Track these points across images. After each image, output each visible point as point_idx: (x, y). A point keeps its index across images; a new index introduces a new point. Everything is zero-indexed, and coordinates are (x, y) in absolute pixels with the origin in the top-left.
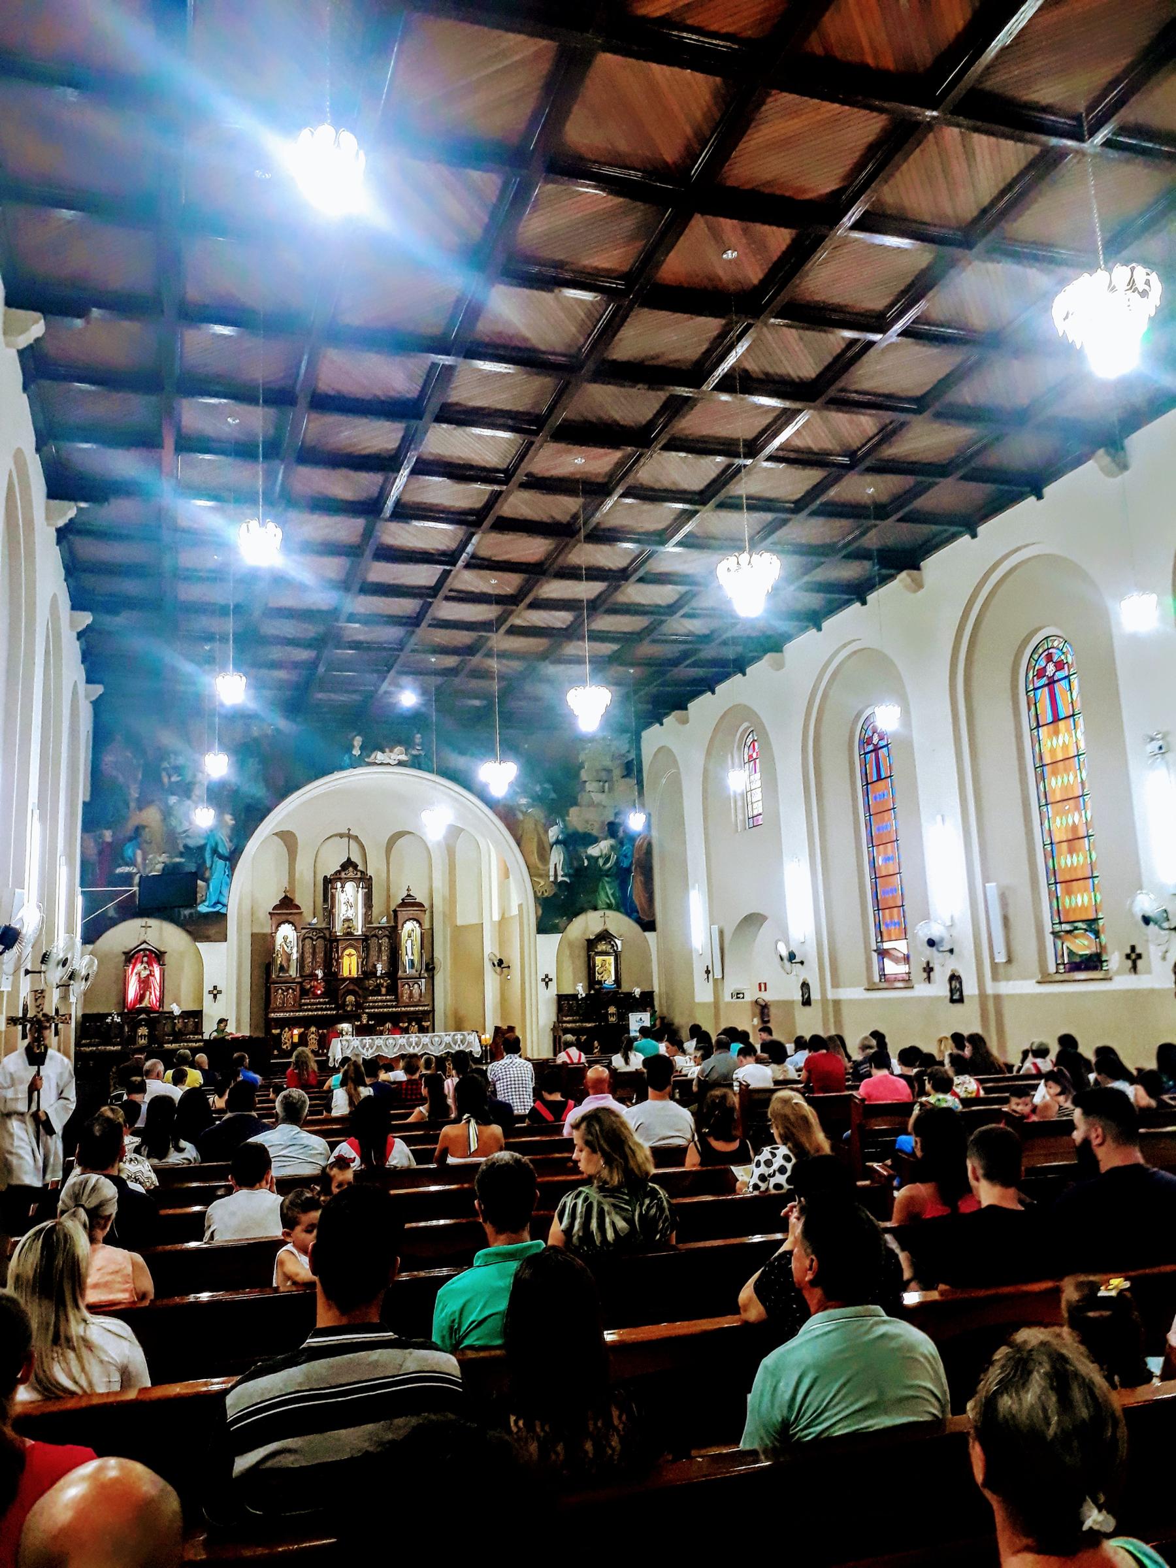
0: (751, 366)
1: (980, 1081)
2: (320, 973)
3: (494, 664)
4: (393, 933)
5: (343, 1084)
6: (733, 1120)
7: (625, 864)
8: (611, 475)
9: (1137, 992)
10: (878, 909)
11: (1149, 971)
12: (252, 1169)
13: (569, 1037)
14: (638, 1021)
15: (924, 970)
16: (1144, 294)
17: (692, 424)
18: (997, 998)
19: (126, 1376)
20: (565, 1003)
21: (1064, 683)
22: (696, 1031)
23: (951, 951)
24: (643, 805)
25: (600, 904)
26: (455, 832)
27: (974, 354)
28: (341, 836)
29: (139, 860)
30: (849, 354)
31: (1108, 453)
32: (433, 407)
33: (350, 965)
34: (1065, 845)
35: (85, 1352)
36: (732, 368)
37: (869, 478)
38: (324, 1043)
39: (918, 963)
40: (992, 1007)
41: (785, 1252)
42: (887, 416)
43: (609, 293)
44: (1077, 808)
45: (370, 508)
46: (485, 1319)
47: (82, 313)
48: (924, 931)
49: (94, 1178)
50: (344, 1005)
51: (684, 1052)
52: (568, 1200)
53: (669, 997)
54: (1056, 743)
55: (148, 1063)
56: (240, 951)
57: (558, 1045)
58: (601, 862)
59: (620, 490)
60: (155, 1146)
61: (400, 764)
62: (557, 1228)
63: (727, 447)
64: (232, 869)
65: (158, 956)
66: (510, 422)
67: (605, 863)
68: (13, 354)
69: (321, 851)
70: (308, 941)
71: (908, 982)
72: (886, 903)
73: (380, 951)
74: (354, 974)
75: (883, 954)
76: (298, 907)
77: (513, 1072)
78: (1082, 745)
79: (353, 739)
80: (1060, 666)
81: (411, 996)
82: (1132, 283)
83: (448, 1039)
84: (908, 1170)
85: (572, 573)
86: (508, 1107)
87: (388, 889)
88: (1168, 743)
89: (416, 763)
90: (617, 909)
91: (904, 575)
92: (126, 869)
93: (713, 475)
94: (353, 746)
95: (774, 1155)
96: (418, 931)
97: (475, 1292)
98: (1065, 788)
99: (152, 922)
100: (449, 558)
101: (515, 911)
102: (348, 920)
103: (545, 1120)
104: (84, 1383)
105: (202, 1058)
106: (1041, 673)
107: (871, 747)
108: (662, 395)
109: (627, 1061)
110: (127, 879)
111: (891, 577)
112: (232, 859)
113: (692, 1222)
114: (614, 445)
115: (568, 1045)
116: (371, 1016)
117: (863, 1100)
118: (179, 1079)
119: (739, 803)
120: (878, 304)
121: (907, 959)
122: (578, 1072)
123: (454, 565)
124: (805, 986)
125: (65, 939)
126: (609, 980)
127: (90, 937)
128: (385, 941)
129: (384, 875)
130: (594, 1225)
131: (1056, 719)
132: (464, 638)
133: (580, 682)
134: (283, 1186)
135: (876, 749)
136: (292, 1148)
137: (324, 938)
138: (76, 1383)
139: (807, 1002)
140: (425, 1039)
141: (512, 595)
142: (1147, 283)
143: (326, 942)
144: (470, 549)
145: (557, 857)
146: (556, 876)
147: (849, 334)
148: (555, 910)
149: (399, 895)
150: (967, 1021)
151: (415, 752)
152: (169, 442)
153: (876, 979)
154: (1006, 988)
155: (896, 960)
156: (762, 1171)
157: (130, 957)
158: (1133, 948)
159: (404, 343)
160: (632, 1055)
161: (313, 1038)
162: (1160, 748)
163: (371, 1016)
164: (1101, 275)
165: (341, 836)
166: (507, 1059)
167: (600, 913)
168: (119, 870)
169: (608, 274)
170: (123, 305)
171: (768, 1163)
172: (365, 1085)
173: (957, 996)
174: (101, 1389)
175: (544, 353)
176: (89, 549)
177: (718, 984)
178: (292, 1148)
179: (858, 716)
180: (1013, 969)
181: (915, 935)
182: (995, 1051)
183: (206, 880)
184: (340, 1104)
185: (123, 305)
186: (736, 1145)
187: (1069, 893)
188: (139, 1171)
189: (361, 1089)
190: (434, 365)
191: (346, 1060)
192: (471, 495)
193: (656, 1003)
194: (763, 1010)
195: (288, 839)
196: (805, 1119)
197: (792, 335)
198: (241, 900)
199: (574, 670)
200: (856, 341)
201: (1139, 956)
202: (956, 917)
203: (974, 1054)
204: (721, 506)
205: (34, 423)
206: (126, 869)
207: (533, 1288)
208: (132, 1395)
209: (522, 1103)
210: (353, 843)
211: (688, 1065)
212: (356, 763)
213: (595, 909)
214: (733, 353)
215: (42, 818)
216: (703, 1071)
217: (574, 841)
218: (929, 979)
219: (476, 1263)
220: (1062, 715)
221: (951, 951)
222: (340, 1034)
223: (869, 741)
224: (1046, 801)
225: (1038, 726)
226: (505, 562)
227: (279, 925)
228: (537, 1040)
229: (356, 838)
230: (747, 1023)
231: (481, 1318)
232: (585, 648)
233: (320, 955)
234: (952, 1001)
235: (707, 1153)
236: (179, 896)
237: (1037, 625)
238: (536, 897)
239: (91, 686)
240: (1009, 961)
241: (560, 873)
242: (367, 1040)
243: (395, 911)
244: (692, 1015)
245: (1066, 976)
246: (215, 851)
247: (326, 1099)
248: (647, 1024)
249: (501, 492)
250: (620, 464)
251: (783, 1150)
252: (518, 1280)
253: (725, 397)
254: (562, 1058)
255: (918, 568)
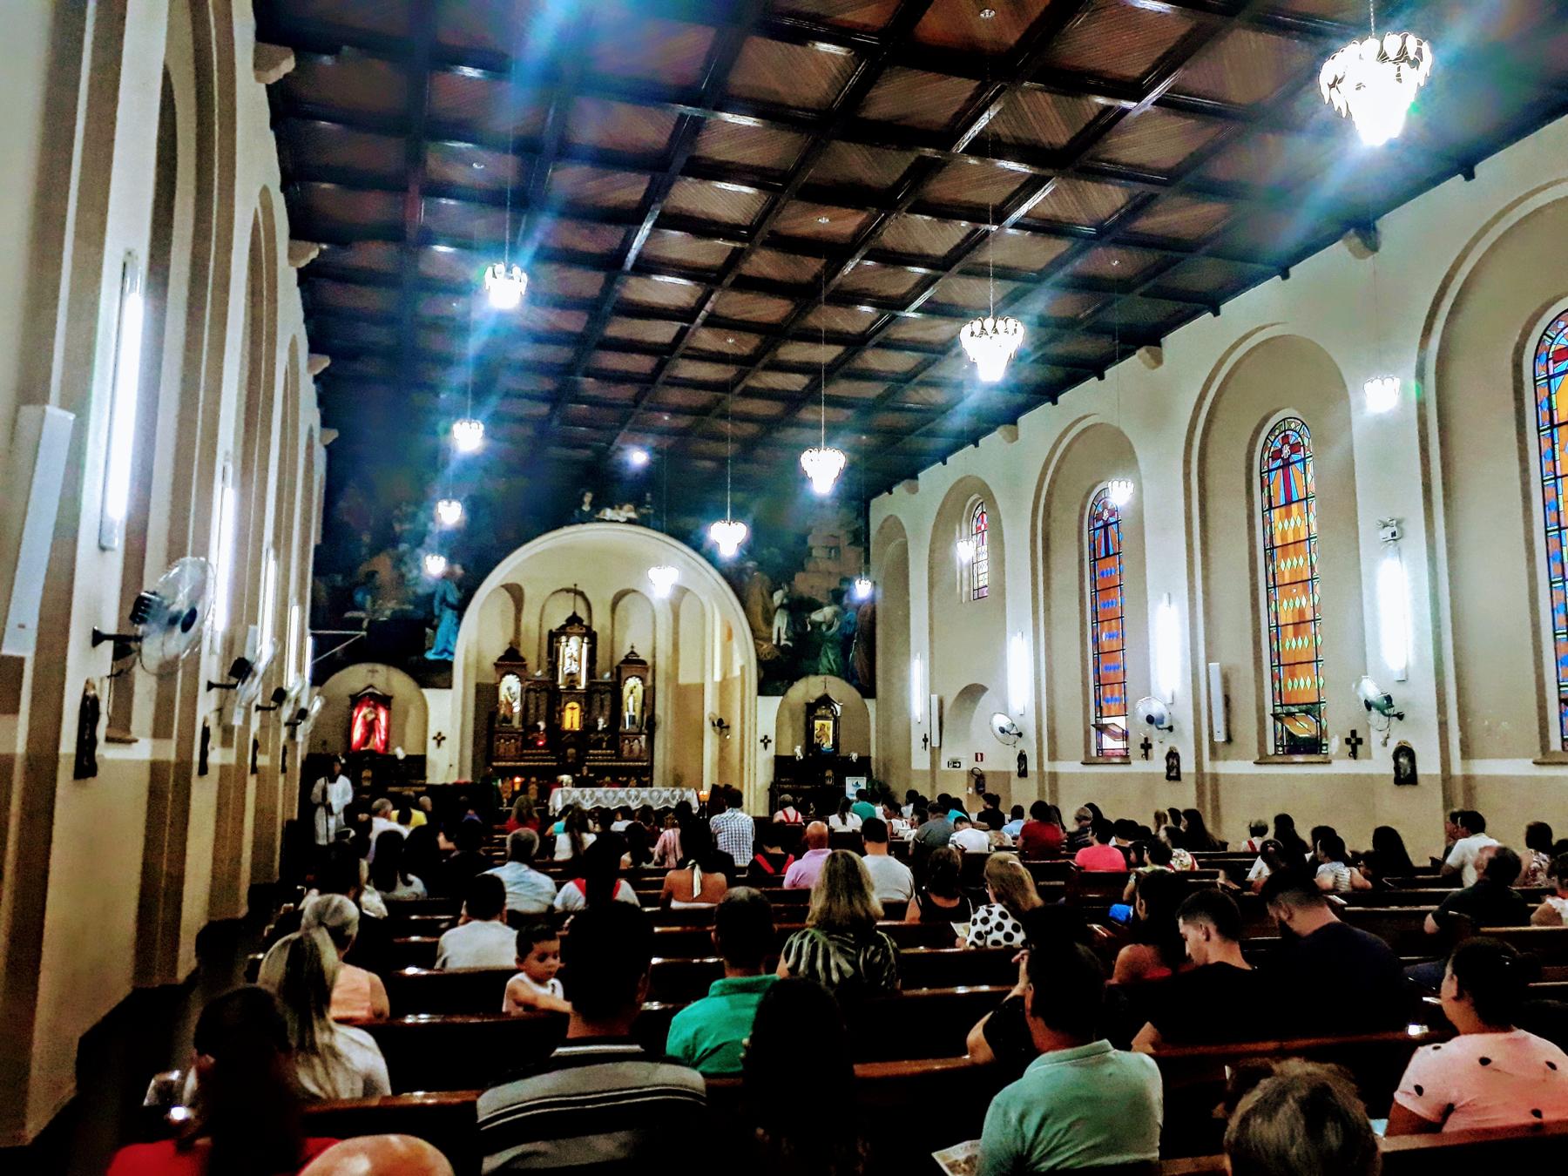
0: (1003, 130)
1: (1196, 857)
2: (542, 725)
3: (728, 427)
4: (616, 689)
5: (566, 830)
6: (948, 879)
7: (849, 630)
8: (856, 235)
9: (1356, 777)
10: (1099, 683)
11: (1369, 756)
12: (489, 902)
13: (788, 797)
14: (853, 786)
15: (1142, 746)
16: (1415, 63)
17: (941, 188)
18: (1215, 778)
19: (370, 1086)
20: (782, 764)
21: (1299, 466)
22: (913, 796)
23: (1170, 729)
24: (868, 573)
25: (822, 669)
26: (681, 592)
27: (1233, 127)
28: (568, 591)
29: (368, 604)
30: (1103, 122)
31: (1357, 234)
32: (680, 161)
33: (572, 718)
34: (1290, 628)
35: (330, 1059)
36: (982, 131)
37: (1114, 251)
38: (545, 794)
39: (1136, 739)
40: (1208, 785)
41: (1016, 997)
42: (1139, 188)
43: (859, 51)
44: (1305, 591)
45: (611, 263)
46: (720, 1047)
47: (334, 50)
48: (1143, 708)
49: (337, 899)
50: (565, 757)
51: (901, 816)
52: (795, 940)
53: (887, 766)
54: (1288, 526)
55: (377, 803)
56: (465, 695)
57: (775, 804)
58: (824, 628)
59: (863, 252)
60: (383, 882)
61: (630, 521)
62: (783, 968)
63: (976, 213)
64: (460, 617)
65: (385, 701)
66: (756, 179)
67: (830, 627)
68: (263, 86)
69: (547, 610)
70: (532, 694)
71: (1125, 759)
72: (1106, 677)
73: (602, 706)
74: (577, 728)
75: (1101, 729)
76: (523, 660)
77: (733, 825)
78: (1314, 529)
79: (583, 495)
80: (1295, 448)
81: (631, 750)
82: (1403, 51)
83: (666, 794)
84: (1131, 931)
85: (813, 337)
86: (729, 858)
87: (612, 641)
88: (1401, 530)
89: (642, 522)
90: (838, 676)
91: (1142, 351)
92: (356, 614)
93: (957, 241)
94: (583, 503)
95: (990, 913)
96: (640, 688)
97: (714, 1018)
98: (1293, 571)
99: (380, 668)
100: (685, 315)
101: (737, 672)
102: (571, 674)
103: (764, 873)
104: (328, 1088)
105: (426, 800)
106: (1277, 455)
107: (1101, 523)
108: (911, 157)
109: (844, 821)
110: (357, 624)
111: (1130, 353)
112: (460, 609)
113: (916, 971)
114: (859, 206)
115: (787, 804)
116: (591, 769)
117: (1079, 868)
118: (404, 819)
119: (965, 574)
120: (1136, 72)
121: (1125, 736)
122: (798, 830)
123: (692, 321)
124: (1022, 758)
125: (296, 681)
126: (828, 744)
127: (319, 678)
128: (608, 698)
129: (608, 632)
130: (819, 964)
131: (1289, 502)
132: (704, 397)
133: (815, 444)
134: (515, 919)
135: (1106, 526)
136: (525, 886)
137: (546, 690)
138: (321, 1088)
139: (1023, 773)
140: (644, 792)
141: (749, 357)
142: (1419, 52)
143: (547, 694)
144: (708, 306)
145: (780, 621)
146: (779, 639)
147: (1101, 100)
148: (775, 675)
149: (621, 655)
150: (1184, 797)
151: (643, 511)
152: (414, 189)
153: (1094, 753)
154: (1226, 767)
155: (1114, 736)
156: (984, 926)
157: (356, 700)
158: (1354, 733)
159: (650, 95)
160: (848, 817)
161: (533, 788)
162: (1394, 534)
163: (591, 769)
164: (1372, 44)
165: (568, 591)
166: (728, 813)
167: (821, 678)
168: (348, 615)
169: (864, 29)
170: (371, 44)
171: (985, 921)
172: (589, 832)
173: (1173, 773)
174: (345, 1095)
175: (790, 107)
176: (334, 294)
177: (935, 753)
178: (525, 886)
179: (1094, 487)
180: (1233, 748)
181: (1135, 714)
182: (1209, 827)
183: (435, 628)
184: (563, 849)
185: (371, 44)
186: (955, 903)
187: (1293, 676)
188: (373, 901)
189: (585, 835)
190: (682, 117)
191: (567, 808)
192: (712, 252)
193: (873, 767)
194: (979, 780)
195: (515, 593)
196: (1021, 881)
197: (1044, 99)
198: (467, 651)
199: (808, 434)
200: (1110, 108)
201: (1360, 741)
202: (1177, 695)
203: (1191, 829)
204: (967, 273)
205: (281, 162)
206: (356, 614)
207: (783, 1012)
208: (375, 1102)
209: (743, 858)
210: (580, 601)
211: (904, 827)
212: (586, 519)
213: (817, 674)
214: (986, 115)
215: (277, 557)
216: (918, 836)
217: (799, 607)
218: (1146, 756)
219: (712, 992)
220: (1295, 498)
221: (1170, 729)
222: (560, 785)
223: (1099, 517)
224: (1274, 584)
225: (1271, 508)
226: (742, 321)
227: (503, 676)
228: (755, 801)
229: (582, 594)
230: (961, 790)
231: (714, 1046)
232: (823, 414)
233: (543, 708)
234: (1169, 778)
235: (927, 907)
236: (410, 645)
237: (1276, 406)
238: (759, 661)
239: (326, 431)
240: (1229, 740)
241: (783, 636)
242: (588, 791)
243: (618, 668)
244: (908, 781)
245: (1285, 758)
246: (444, 600)
247: (549, 844)
248: (863, 787)
249: (742, 250)
250: (862, 227)
251: (998, 908)
252: (762, 1009)
253: (972, 161)
254: (779, 816)
255: (1159, 345)
